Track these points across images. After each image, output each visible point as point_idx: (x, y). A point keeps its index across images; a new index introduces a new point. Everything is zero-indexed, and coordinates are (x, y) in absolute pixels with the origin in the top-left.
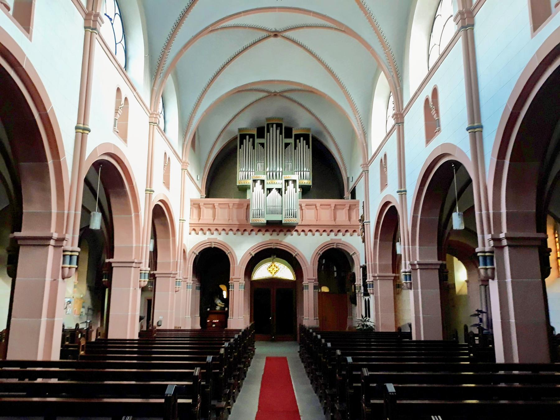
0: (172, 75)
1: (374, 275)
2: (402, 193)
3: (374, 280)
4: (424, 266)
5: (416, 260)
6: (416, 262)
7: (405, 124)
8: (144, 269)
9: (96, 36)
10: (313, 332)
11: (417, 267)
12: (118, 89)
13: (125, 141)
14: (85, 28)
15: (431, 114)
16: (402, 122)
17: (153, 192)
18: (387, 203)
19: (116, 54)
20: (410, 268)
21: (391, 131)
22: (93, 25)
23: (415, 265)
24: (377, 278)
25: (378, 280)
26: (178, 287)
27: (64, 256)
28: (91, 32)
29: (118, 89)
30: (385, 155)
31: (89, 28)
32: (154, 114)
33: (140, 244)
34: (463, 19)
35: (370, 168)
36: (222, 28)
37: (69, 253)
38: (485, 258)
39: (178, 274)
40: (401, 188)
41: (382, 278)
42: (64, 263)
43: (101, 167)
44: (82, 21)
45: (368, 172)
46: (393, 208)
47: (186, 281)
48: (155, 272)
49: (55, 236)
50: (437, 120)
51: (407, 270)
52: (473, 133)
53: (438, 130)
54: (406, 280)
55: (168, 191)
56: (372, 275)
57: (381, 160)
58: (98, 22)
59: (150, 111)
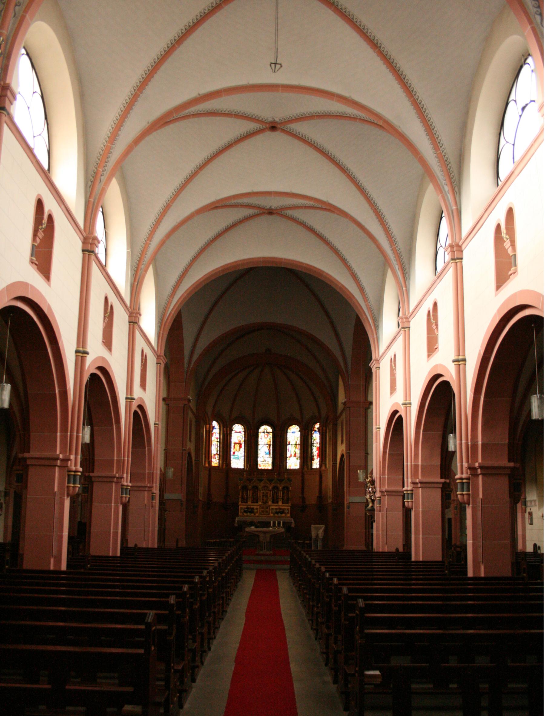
0: (152, 266)
1: (414, 481)
2: (460, 362)
3: (381, 495)
4: (425, 484)
5: (477, 462)
6: (477, 465)
7: (464, 261)
9: (93, 257)
11: (479, 471)
17: (88, 353)
18: (396, 412)
20: (469, 473)
22: (91, 248)
23: (417, 483)
24: (419, 485)
25: (386, 496)
26: (125, 496)
27: (69, 475)
30: (435, 305)
31: (132, 322)
33: (151, 471)
34: (453, 252)
35: (413, 323)
37: (125, 487)
38: (462, 483)
40: (406, 400)
41: (425, 484)
42: (69, 483)
44: (127, 317)
45: (409, 330)
47: (151, 491)
48: (91, 474)
49: (61, 456)
50: (513, 256)
51: (464, 476)
52: (458, 365)
53: (514, 272)
54: (463, 491)
55: (144, 393)
56: (468, 464)
58: (8, 98)
59: (157, 353)
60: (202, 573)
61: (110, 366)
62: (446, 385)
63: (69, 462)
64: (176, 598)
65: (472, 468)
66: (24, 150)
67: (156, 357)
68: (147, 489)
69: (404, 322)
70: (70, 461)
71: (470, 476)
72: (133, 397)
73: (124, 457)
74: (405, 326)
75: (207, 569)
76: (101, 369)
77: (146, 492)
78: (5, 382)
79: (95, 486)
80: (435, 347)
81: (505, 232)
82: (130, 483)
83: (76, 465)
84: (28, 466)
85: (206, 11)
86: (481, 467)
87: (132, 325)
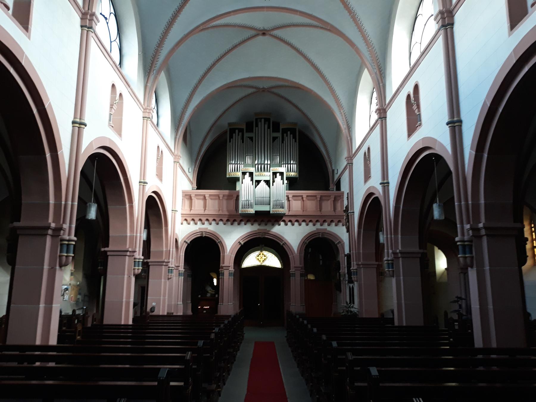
2: (385, 184)
6: (398, 251)
7: (388, 119)
9: (91, 34)
11: (400, 255)
13: (120, 135)
14: (82, 26)
15: (413, 109)
16: (385, 116)
17: (147, 183)
20: (393, 257)
21: (374, 125)
23: (360, 265)
24: (361, 266)
25: (362, 268)
28: (87, 31)
30: (369, 149)
32: (147, 109)
33: (134, 233)
34: (443, 18)
35: (355, 161)
37: (66, 243)
40: (384, 180)
42: (135, 266)
43: (96, 160)
47: (178, 269)
49: (53, 225)
50: (418, 115)
56: (392, 251)
58: (94, 21)
59: (143, 106)
60: (220, 326)
61: (161, 191)
62: (377, 199)
63: (62, 232)
64: (193, 353)
65: (394, 253)
66: (168, 150)
67: (81, 15)
68: (128, 253)
69: (445, 18)
70: (63, 230)
71: (394, 258)
72: (83, 121)
73: (136, 233)
74: (350, 163)
75: (223, 323)
76: (154, 192)
77: (127, 257)
78: (93, 202)
79: (151, 267)
80: (369, 176)
81: (413, 99)
82: (75, 236)
83: (139, 255)
84: (108, 256)
85: (230, 49)
86: (401, 253)
87: (86, 32)
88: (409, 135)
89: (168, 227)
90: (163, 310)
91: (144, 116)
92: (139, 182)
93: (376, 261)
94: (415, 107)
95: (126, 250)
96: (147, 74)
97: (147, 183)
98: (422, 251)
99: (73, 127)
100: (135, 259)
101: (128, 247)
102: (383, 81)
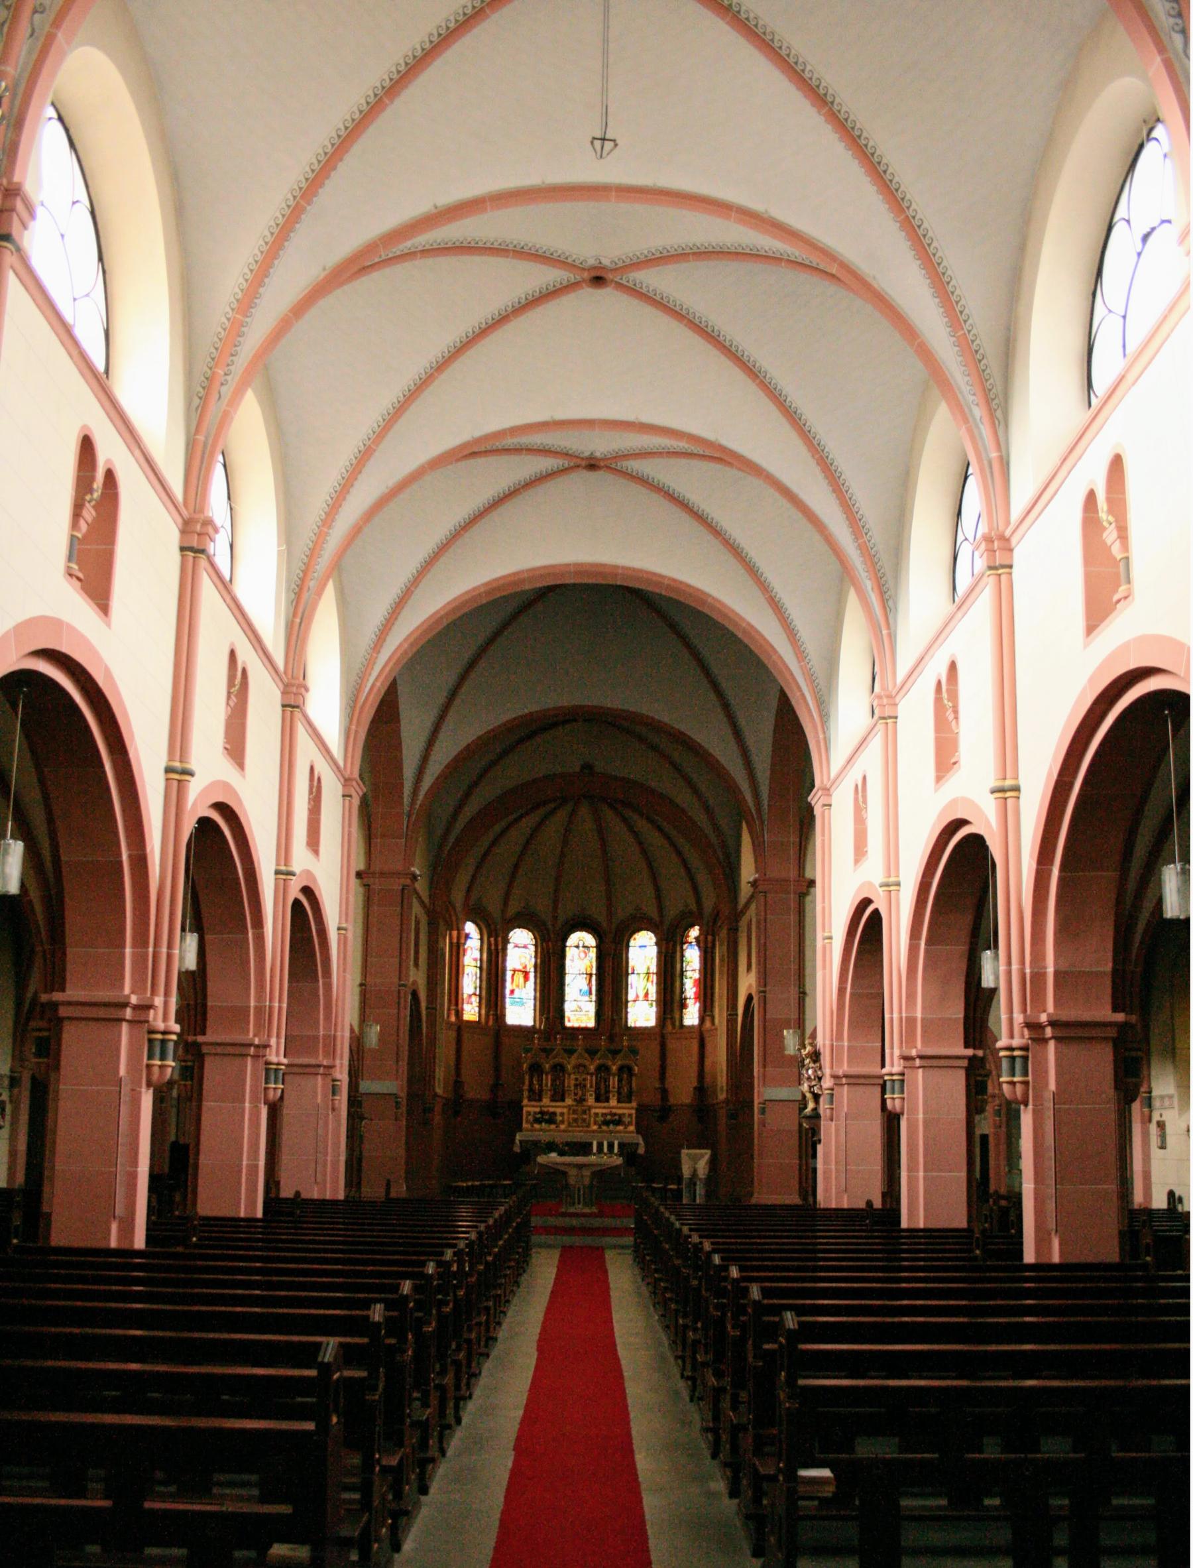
0: (334, 582)
2: (1007, 792)
3: (905, 1067)
5: (1044, 1011)
6: (1043, 1018)
8: (161, 1026)
9: (203, 562)
10: (714, 1251)
11: (1049, 1032)
12: (232, 654)
13: (104, 607)
14: (182, 549)
15: (1104, 543)
16: (1007, 562)
17: (191, 774)
18: (866, 902)
19: (107, 377)
20: (1027, 1037)
21: (972, 590)
24: (918, 1062)
27: (150, 1041)
28: (194, 557)
29: (232, 654)
30: (953, 667)
32: (292, 685)
34: (991, 551)
36: (426, 252)
37: (274, 1067)
39: (338, 1068)
42: (150, 1057)
43: (24, 692)
44: (278, 694)
46: (876, 913)
49: (134, 1000)
51: (1016, 1042)
56: (1025, 1017)
57: (939, 683)
58: (18, 215)
63: (152, 1012)
65: (1033, 1026)
68: (321, 1070)
71: (1030, 1042)
74: (886, 715)
76: (221, 807)
78: (12, 837)
79: (209, 1063)
80: (953, 760)
84: (60, 1020)
85: (452, 25)
86: (1053, 1023)
88: (1090, 629)
89: (265, 930)
90: (252, 1203)
91: (285, 703)
92: (273, 872)
93: (967, 1046)
94: (951, 716)
95: (248, 1042)
96: (196, 401)
97: (191, 774)
98: (970, 1052)
99: (167, 779)
100: (151, 1032)
101: (127, 990)
102: (891, 621)
